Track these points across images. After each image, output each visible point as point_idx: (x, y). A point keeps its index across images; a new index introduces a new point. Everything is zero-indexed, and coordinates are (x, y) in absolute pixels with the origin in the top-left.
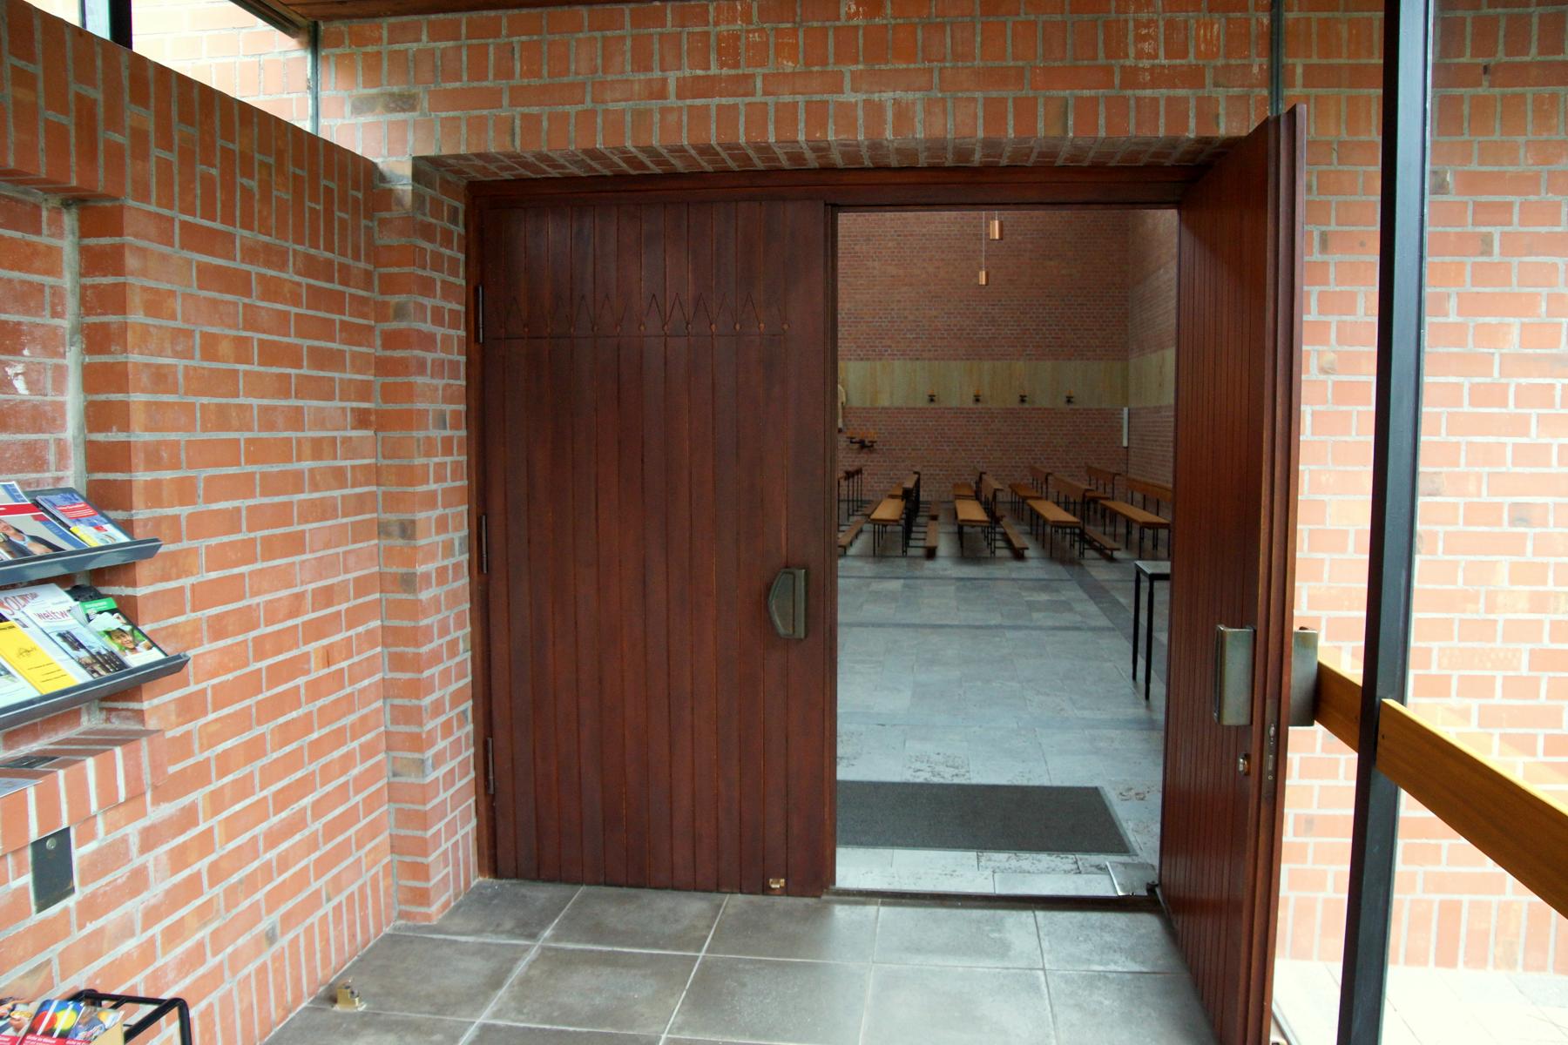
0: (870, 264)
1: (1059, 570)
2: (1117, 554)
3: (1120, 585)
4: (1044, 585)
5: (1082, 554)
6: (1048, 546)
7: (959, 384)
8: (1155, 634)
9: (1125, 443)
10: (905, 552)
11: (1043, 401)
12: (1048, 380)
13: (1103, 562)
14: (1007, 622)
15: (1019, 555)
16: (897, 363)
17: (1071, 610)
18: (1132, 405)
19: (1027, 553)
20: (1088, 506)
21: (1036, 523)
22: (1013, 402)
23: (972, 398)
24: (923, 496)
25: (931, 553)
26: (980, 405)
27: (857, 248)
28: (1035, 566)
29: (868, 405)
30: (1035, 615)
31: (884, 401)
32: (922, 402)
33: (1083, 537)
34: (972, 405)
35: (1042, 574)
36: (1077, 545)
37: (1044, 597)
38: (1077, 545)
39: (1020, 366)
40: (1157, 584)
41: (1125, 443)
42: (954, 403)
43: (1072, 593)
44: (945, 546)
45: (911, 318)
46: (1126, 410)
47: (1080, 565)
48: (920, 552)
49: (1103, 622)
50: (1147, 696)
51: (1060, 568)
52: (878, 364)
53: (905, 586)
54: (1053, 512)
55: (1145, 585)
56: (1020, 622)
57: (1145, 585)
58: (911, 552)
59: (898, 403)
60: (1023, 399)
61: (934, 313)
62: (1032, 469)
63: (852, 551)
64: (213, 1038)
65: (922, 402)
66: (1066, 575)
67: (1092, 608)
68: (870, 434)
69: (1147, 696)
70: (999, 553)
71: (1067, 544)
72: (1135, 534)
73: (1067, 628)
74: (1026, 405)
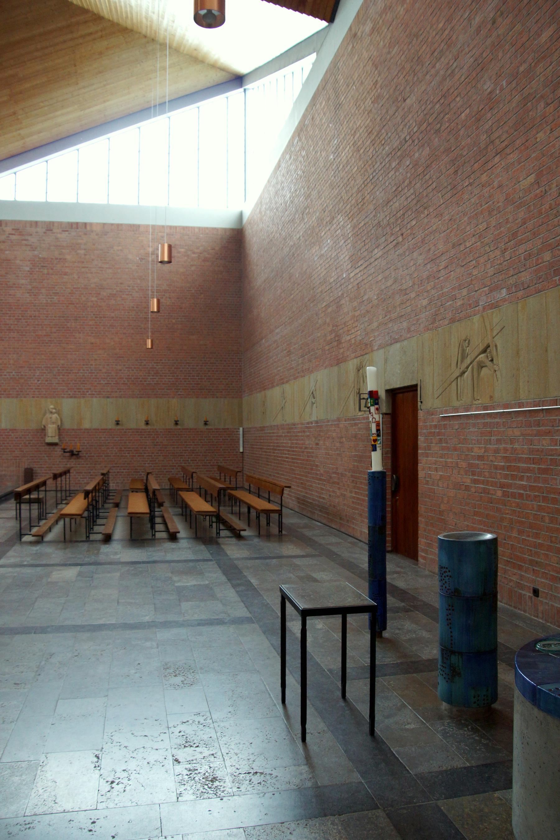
0: (77, 335)
1: (203, 551)
2: (242, 533)
3: (250, 563)
4: (190, 568)
5: (218, 533)
6: (194, 525)
7: (135, 413)
8: (288, 624)
9: (241, 450)
10: (88, 537)
11: (189, 423)
12: (192, 411)
13: (234, 541)
14: (161, 618)
15: (173, 537)
16: (95, 400)
17: (213, 597)
18: (246, 426)
19: (179, 535)
20: (221, 497)
21: (187, 514)
22: (170, 425)
23: (144, 422)
24: (112, 486)
25: (108, 539)
26: (149, 427)
27: (69, 325)
28: (185, 549)
29: (75, 427)
30: (185, 605)
31: (86, 425)
32: (111, 425)
33: (220, 519)
34: (143, 426)
35: (191, 557)
36: (214, 525)
37: (190, 582)
38: (214, 525)
39: (174, 401)
40: (311, 621)
41: (241, 450)
42: (133, 426)
43: (214, 575)
44: (120, 530)
45: (104, 371)
46: (241, 429)
47: (218, 544)
48: (100, 537)
49: (242, 611)
50: (304, 739)
51: (203, 547)
52: (82, 401)
53: (80, 574)
54: (198, 504)
55: (294, 626)
56: (171, 617)
57: (294, 626)
58: (93, 537)
59: (95, 425)
60: (176, 423)
61: (119, 367)
62: (183, 468)
63: (49, 537)
64: (2, 569)
65: (111, 425)
66: (208, 556)
67: (231, 594)
68: (77, 446)
69: (304, 739)
70: (158, 535)
71: (207, 523)
72: (253, 514)
73: (210, 623)
74: (179, 427)
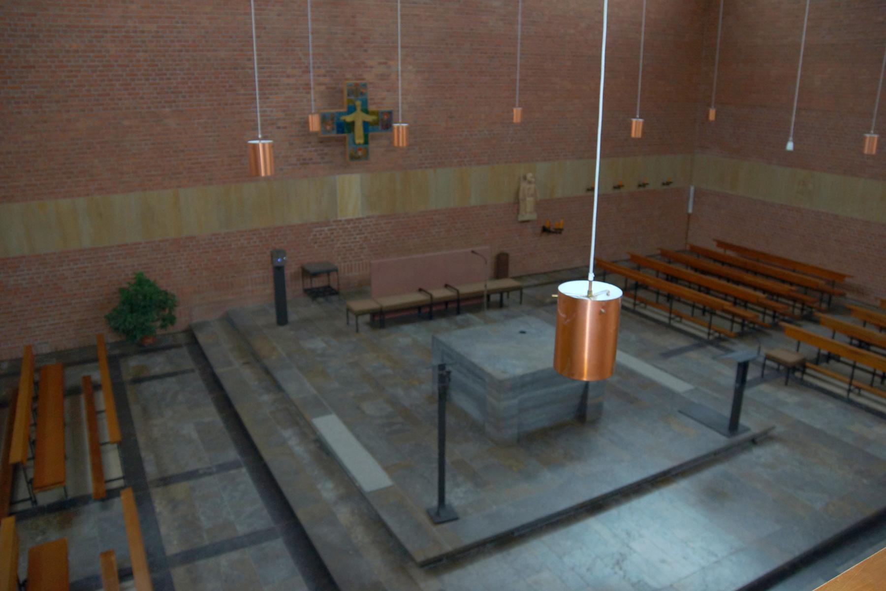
46: (692, 189)
